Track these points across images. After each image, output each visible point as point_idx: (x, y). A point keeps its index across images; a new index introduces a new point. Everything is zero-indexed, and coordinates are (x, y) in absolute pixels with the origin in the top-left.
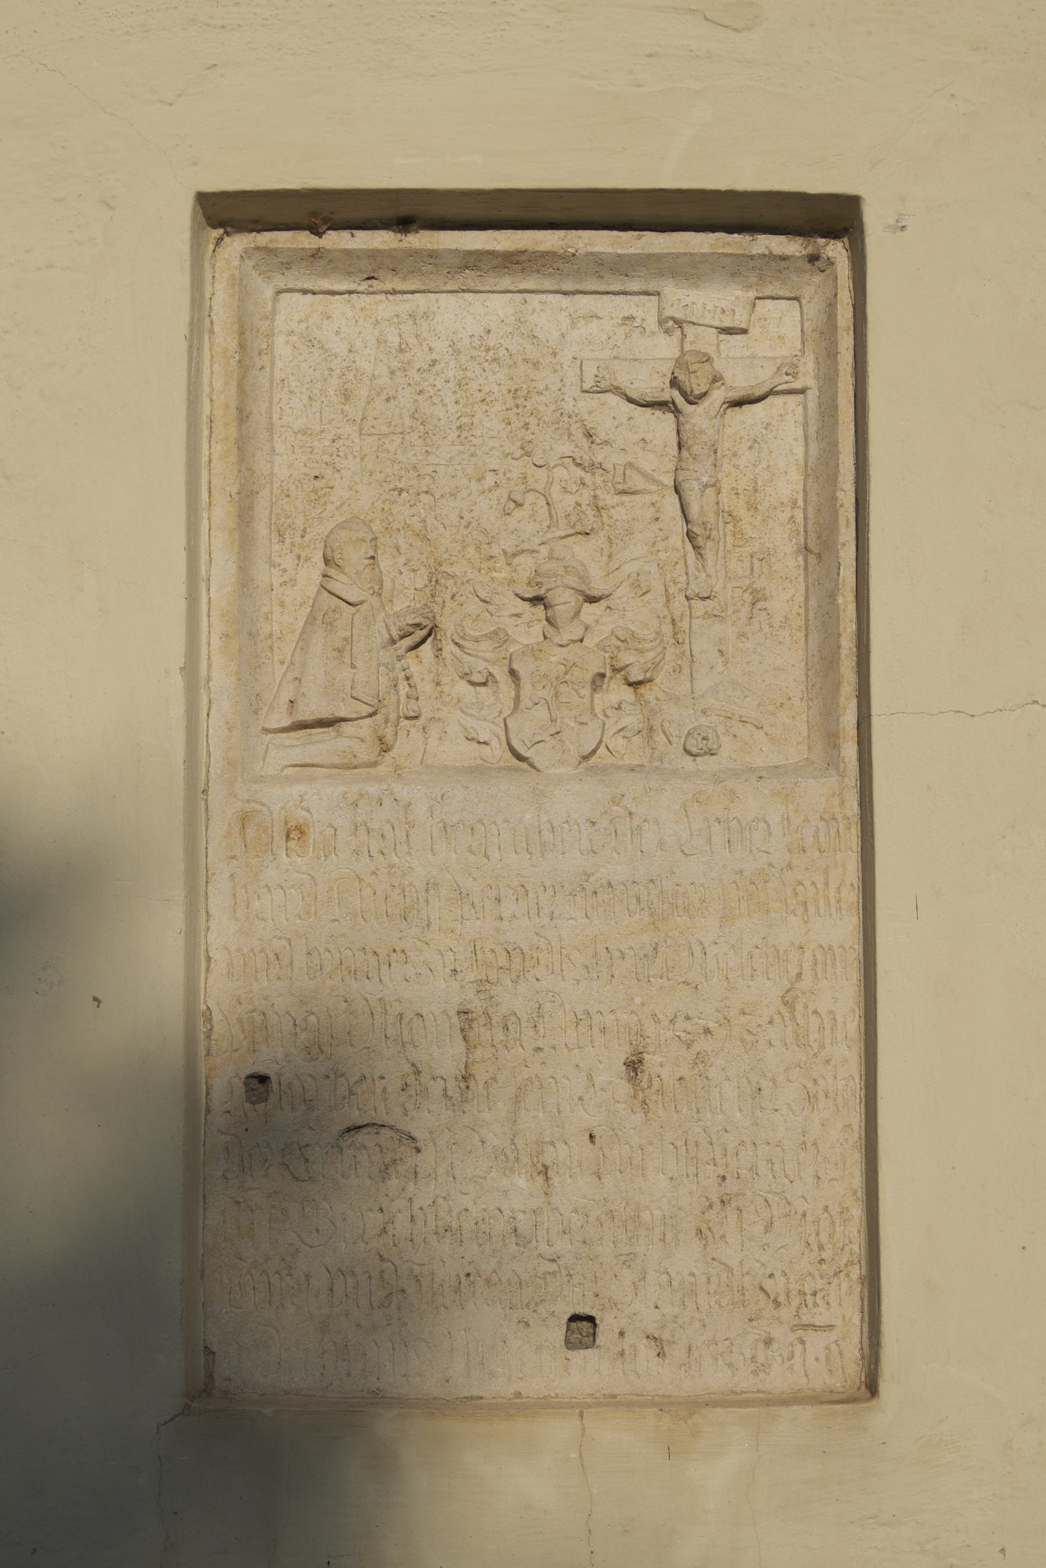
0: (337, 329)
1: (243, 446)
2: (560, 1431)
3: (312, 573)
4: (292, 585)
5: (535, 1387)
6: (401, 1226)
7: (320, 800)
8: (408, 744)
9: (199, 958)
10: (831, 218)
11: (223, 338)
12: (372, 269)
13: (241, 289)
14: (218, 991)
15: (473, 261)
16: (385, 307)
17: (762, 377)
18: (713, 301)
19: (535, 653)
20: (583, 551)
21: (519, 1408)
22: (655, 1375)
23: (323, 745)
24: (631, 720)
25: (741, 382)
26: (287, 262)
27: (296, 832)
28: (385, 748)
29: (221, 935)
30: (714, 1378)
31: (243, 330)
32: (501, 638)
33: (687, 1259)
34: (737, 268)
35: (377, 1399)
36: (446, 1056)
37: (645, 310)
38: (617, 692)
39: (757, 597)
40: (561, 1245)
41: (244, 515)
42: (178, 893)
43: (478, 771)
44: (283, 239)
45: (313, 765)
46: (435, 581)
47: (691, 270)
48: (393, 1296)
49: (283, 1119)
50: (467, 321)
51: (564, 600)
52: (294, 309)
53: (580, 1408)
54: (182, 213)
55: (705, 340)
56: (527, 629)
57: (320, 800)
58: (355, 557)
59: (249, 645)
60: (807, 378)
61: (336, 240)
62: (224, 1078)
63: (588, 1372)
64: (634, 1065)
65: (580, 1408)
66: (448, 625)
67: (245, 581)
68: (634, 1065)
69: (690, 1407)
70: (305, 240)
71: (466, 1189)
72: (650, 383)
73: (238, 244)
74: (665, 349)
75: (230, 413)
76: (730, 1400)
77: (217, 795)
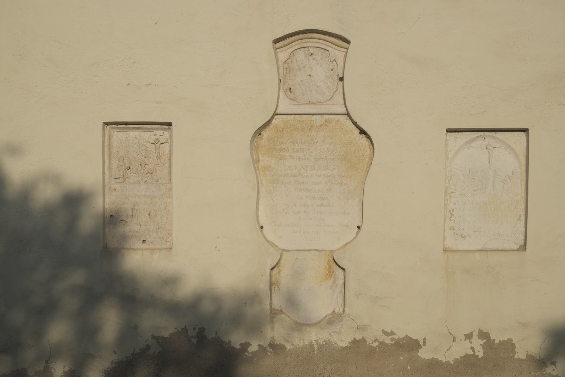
0: (119, 135)
1: (110, 149)
2: (140, 252)
3: (117, 162)
4: (115, 163)
5: (139, 247)
6: (126, 231)
7: (117, 186)
8: (127, 180)
9: (100, 204)
10: (170, 124)
11: (107, 137)
12: (123, 129)
13: (109, 131)
14: (107, 206)
15: (134, 128)
16: (125, 133)
17: (164, 141)
18: (159, 132)
19: (140, 171)
20: (145, 159)
21: (138, 249)
22: (152, 246)
23: (118, 180)
24: (150, 178)
25: (162, 141)
26: (115, 128)
27: (115, 190)
28: (124, 181)
29: (107, 201)
30: (158, 246)
31: (109, 136)
32: (137, 169)
33: (155, 234)
34: (161, 129)
35: (123, 248)
36: (130, 213)
37: (152, 133)
38: (149, 175)
39: (164, 164)
40: (142, 233)
41: (110, 156)
42: (102, 196)
43: (134, 183)
44: (114, 126)
45: (278, 102)
46: (130, 163)
47: (157, 129)
48: (124, 238)
49: (112, 220)
50: (133, 134)
51: (143, 165)
52: (115, 133)
53: (143, 249)
54: (102, 124)
55: (158, 137)
56: (139, 168)
57: (117, 186)
58: (121, 160)
59: (110, 170)
60: (169, 141)
61: (119, 126)
62: (108, 215)
63: (145, 246)
64: (149, 214)
65: (143, 249)
66: (131, 167)
67: (110, 163)
68: (149, 214)
69: (153, 250)
70: (116, 126)
71: (132, 227)
72: (152, 141)
73: (109, 127)
74: (154, 137)
75: (107, 146)
76: (158, 249)
77: (107, 186)
